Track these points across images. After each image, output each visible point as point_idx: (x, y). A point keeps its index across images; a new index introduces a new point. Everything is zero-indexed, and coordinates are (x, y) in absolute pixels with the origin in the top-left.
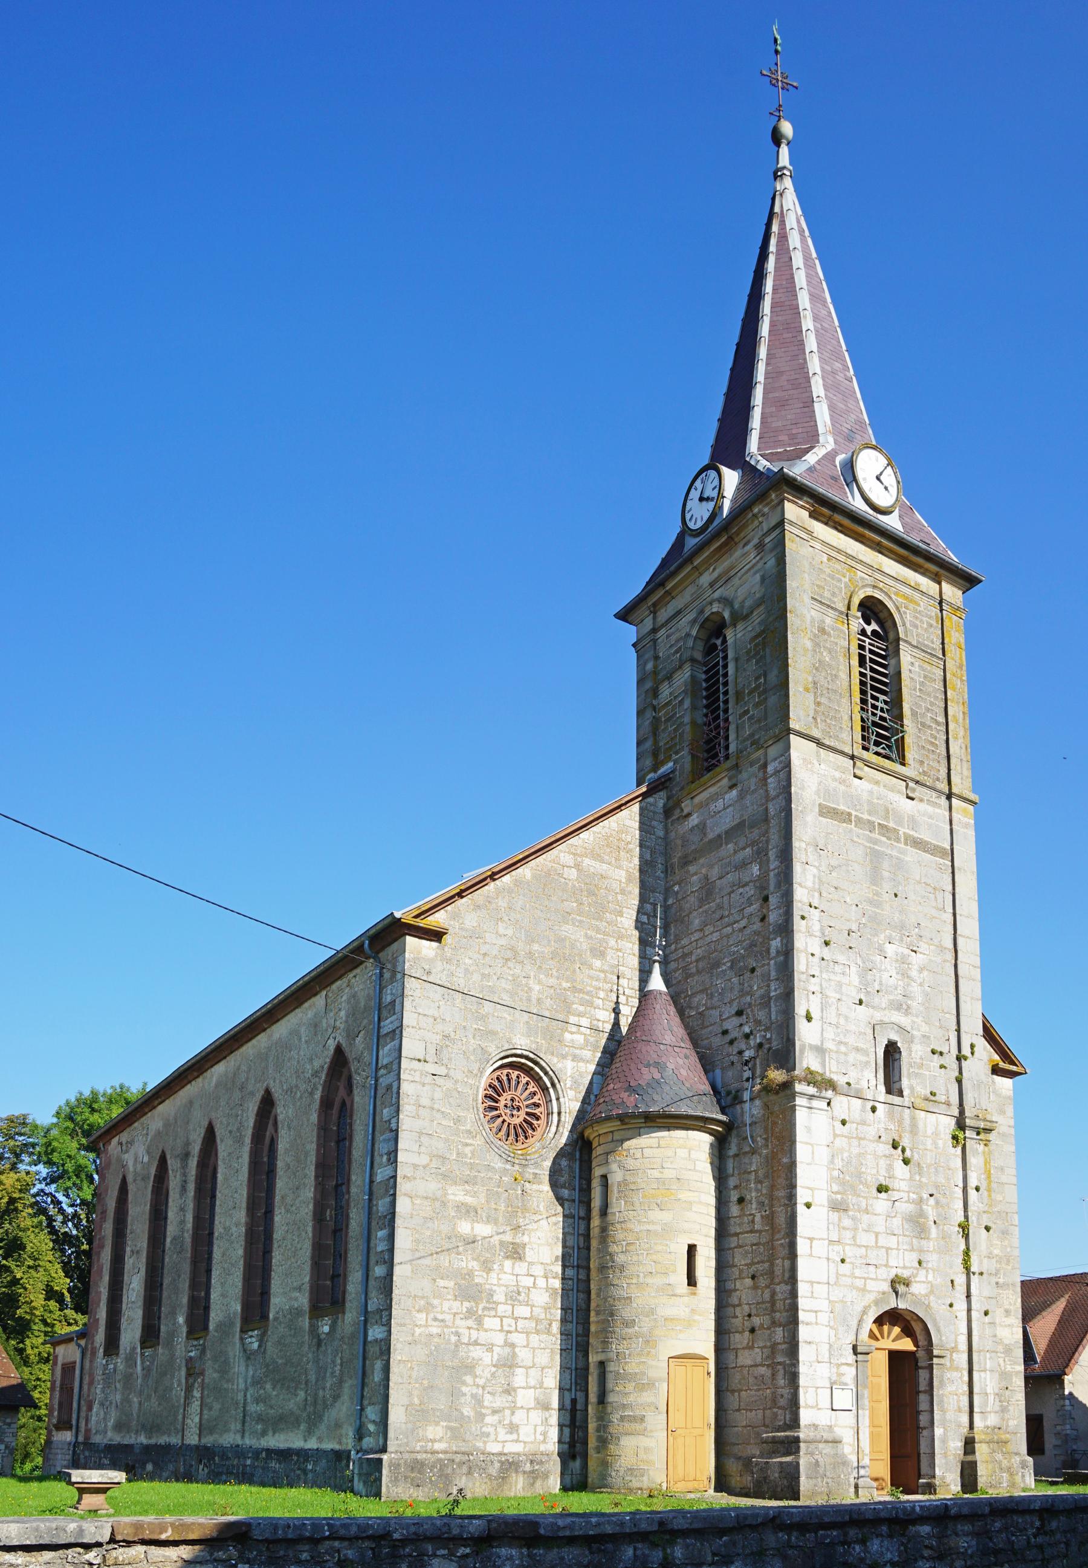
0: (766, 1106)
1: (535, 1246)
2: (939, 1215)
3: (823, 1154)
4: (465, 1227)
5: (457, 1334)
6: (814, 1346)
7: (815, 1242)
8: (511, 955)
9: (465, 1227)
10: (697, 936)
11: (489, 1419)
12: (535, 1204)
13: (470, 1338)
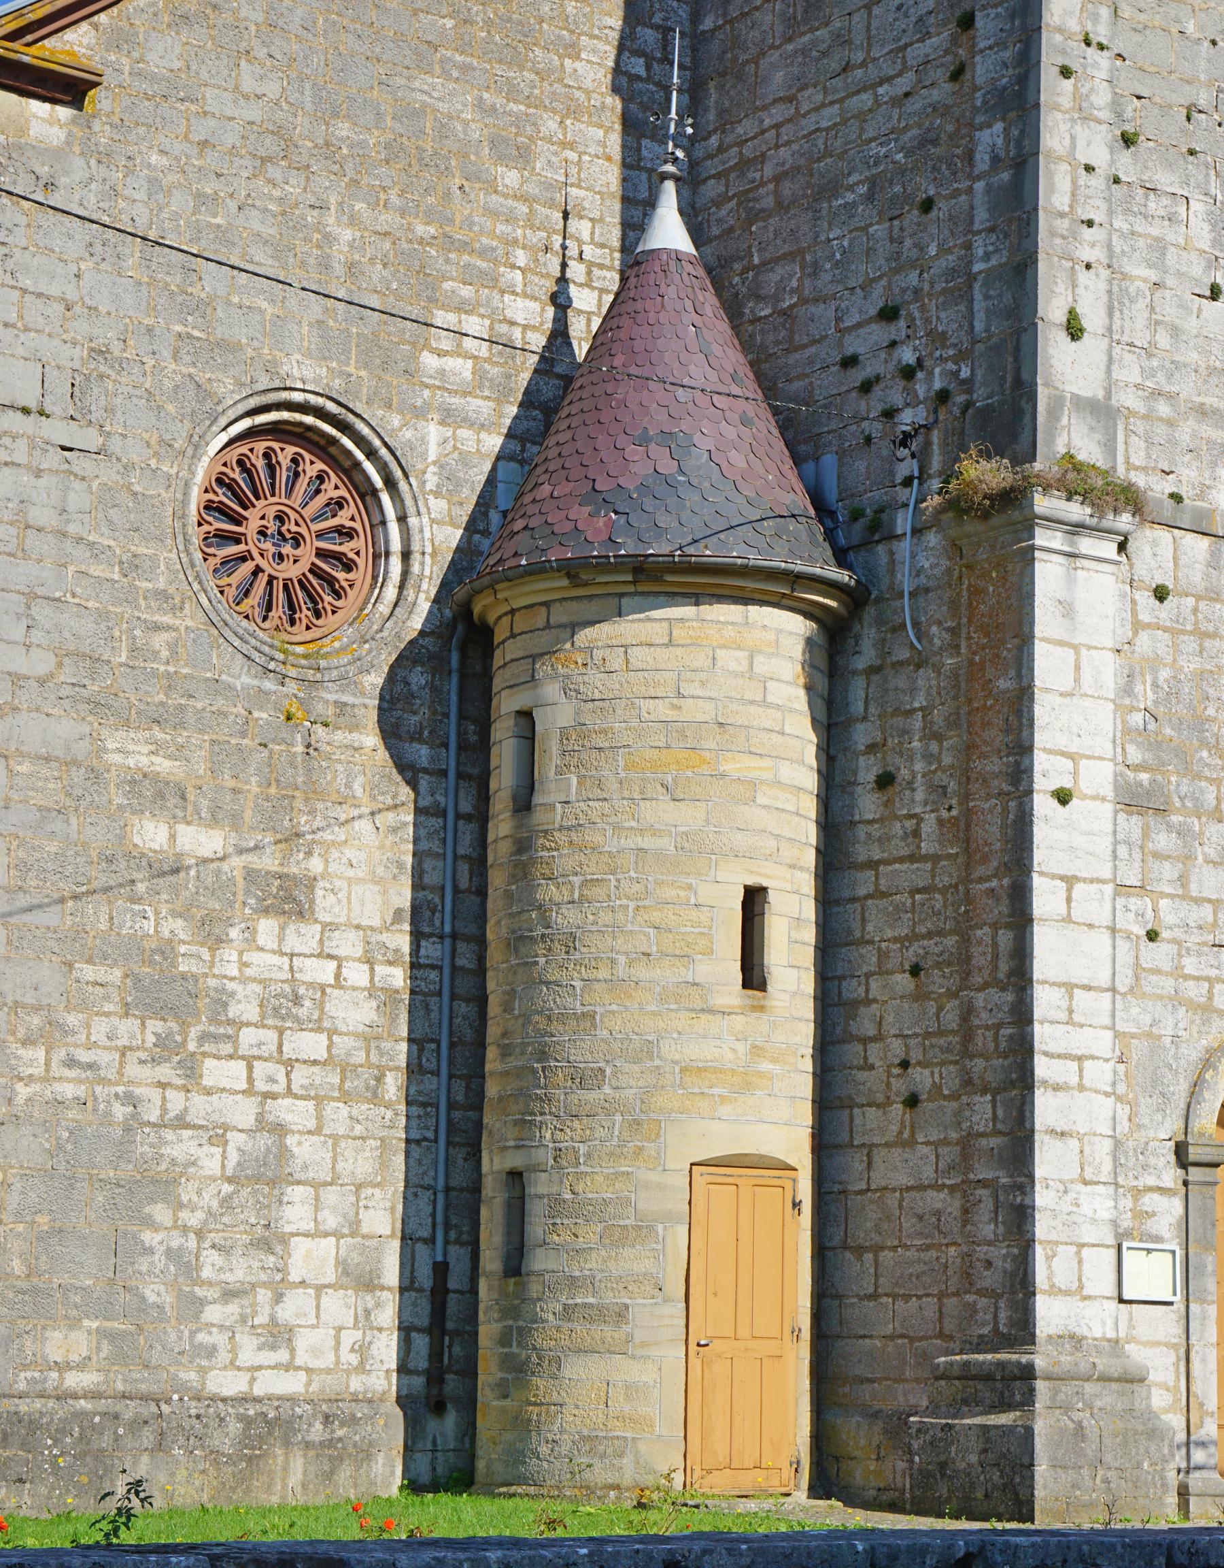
0: (955, 548)
1: (338, 883)
3: (1104, 671)
4: (152, 834)
5: (131, 1100)
6: (1074, 1143)
8: (277, 148)
9: (152, 834)
10: (779, 113)
11: (213, 1313)
12: (341, 779)
13: (164, 1110)
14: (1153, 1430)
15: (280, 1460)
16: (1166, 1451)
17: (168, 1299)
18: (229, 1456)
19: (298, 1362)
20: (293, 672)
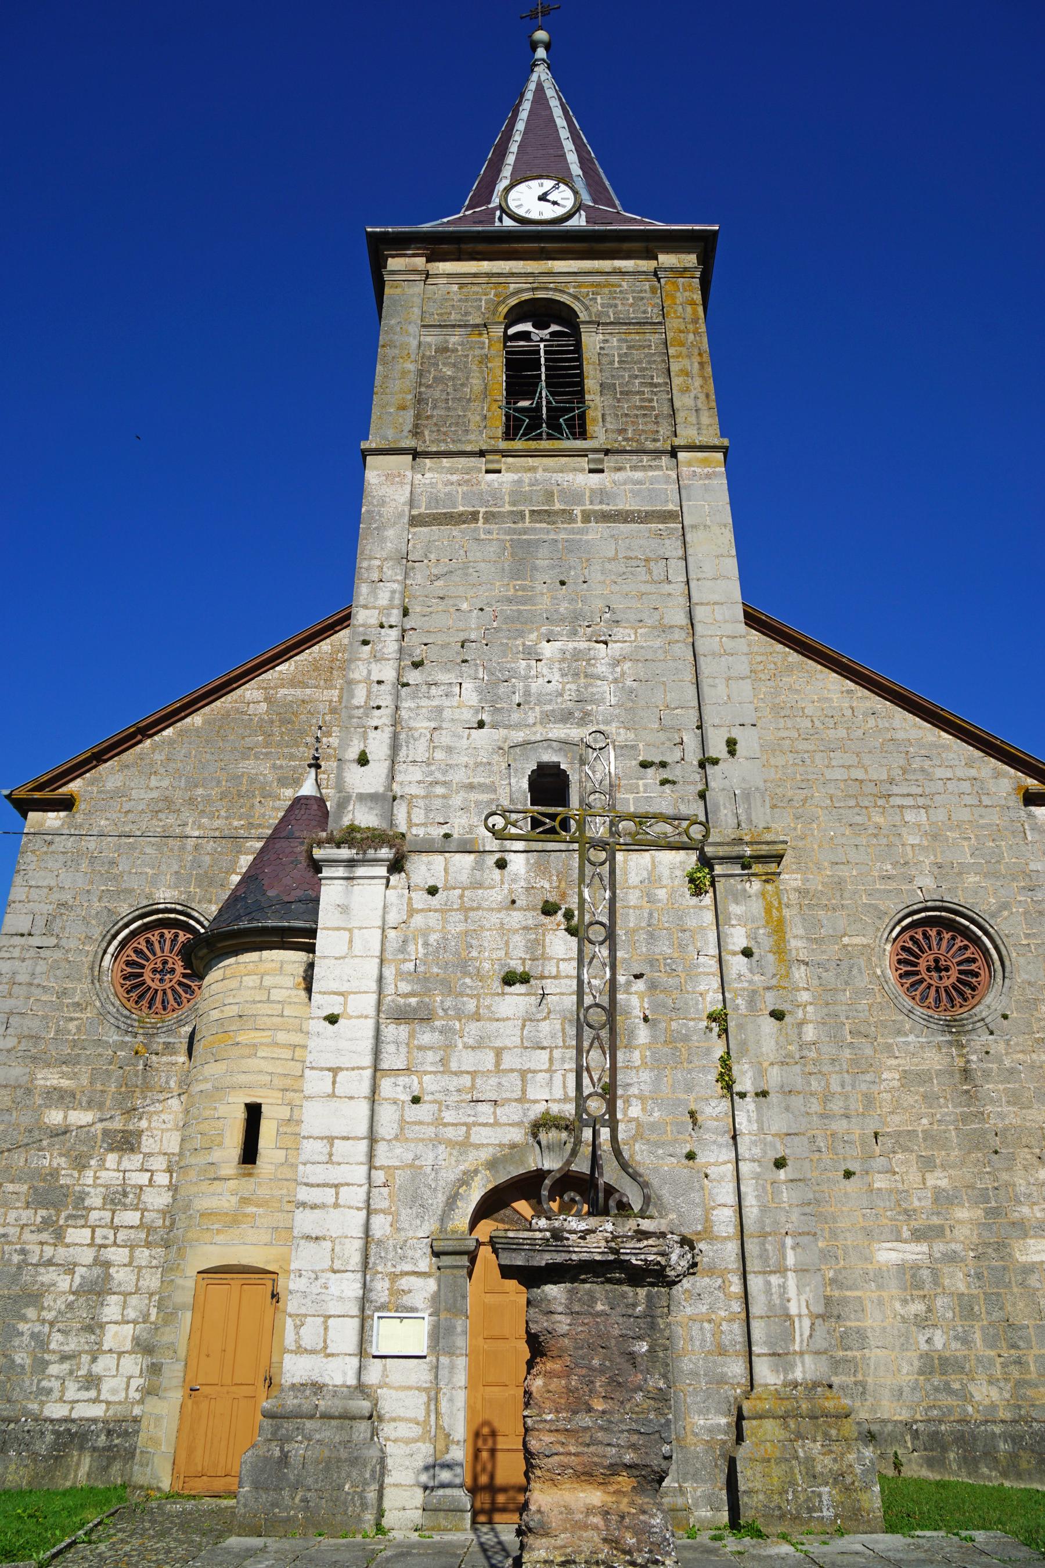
1: (155, 1132)
2: (655, 1006)
5: (23, 1252)
6: (327, 1245)
7: (341, 1076)
9: (55, 1117)
11: (54, 1369)
12: (163, 1080)
13: (41, 1257)
14: (356, 1458)
15: (75, 1459)
16: (368, 1476)
17: (28, 1361)
18: (44, 1456)
19: (102, 1398)
20: (141, 1031)
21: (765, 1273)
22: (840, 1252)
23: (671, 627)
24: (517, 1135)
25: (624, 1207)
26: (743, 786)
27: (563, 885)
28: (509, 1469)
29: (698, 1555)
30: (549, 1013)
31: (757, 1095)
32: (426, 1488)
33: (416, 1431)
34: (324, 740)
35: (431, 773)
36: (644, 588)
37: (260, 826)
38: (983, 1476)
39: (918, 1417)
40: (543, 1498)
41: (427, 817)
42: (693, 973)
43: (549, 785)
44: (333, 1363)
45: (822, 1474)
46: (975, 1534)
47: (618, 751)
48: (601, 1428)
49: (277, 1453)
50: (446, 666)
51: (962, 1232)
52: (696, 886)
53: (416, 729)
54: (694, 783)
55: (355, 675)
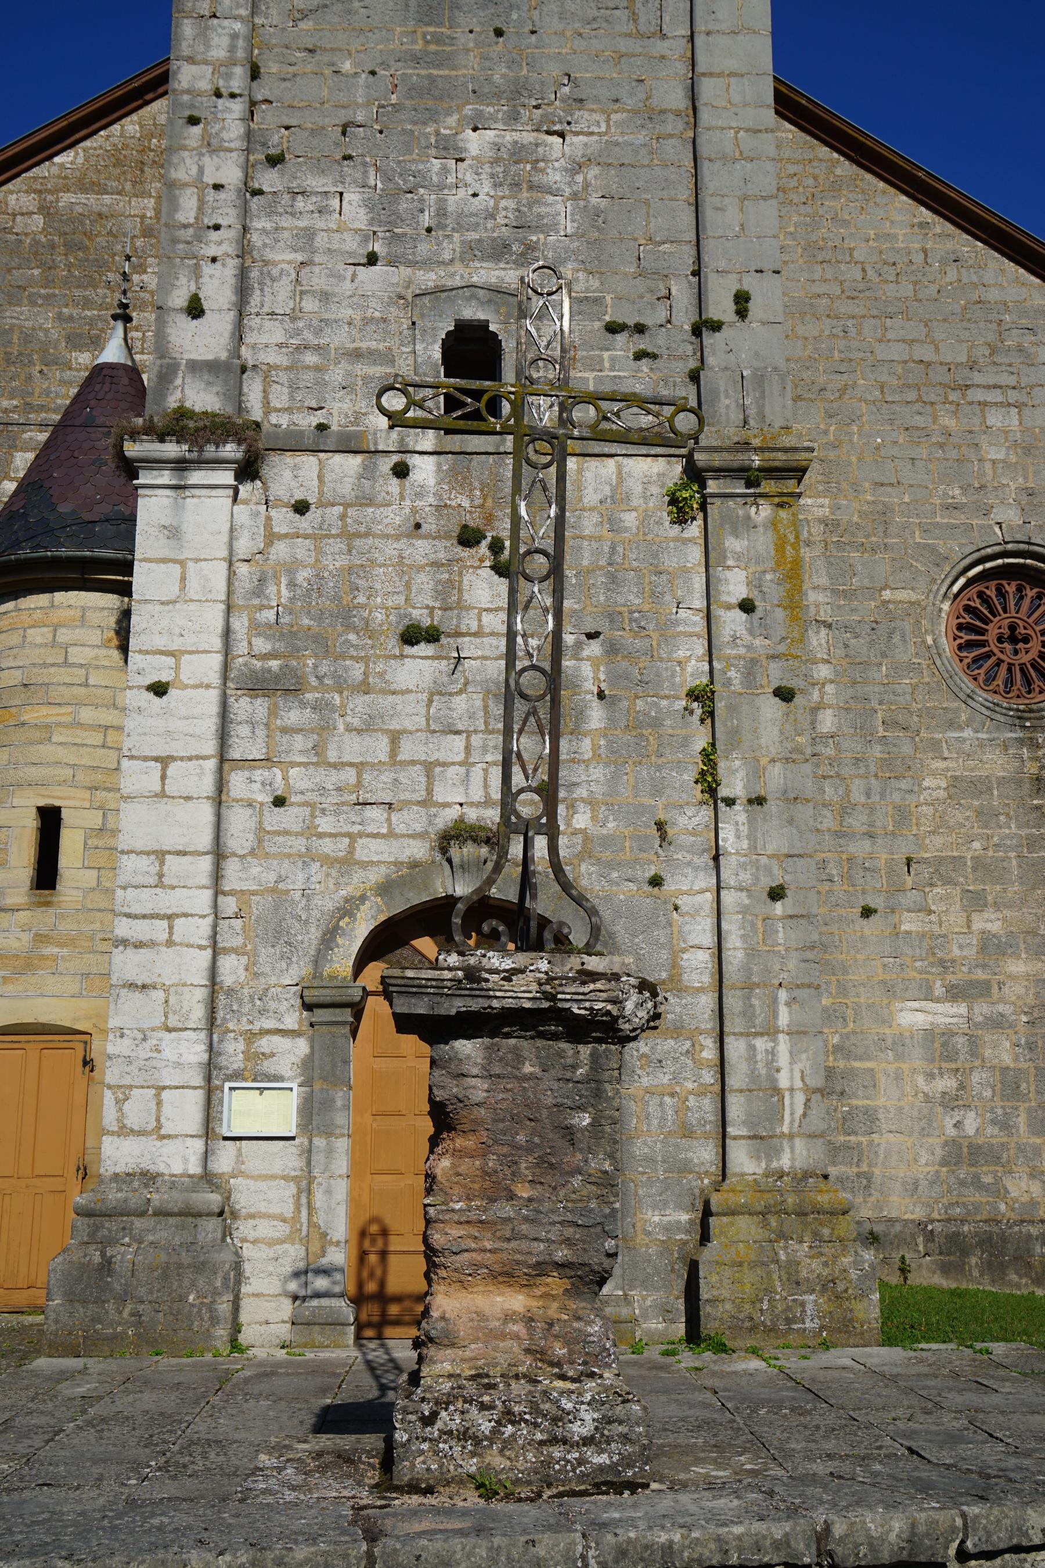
2: (614, 678)
6: (159, 995)
7: (173, 769)
14: (203, 1263)
16: (218, 1284)
21: (748, 1035)
22: (850, 1012)
23: (663, 112)
24: (420, 850)
25: (562, 943)
26: (756, 364)
27: (489, 503)
28: (404, 1274)
29: (644, 1372)
30: (466, 684)
31: (750, 801)
32: (295, 1298)
33: (282, 1230)
34: (136, 278)
35: (298, 332)
36: (623, 45)
37: (42, 408)
38: (1011, 1284)
39: (935, 1215)
40: (447, 1303)
41: (292, 398)
42: (670, 632)
43: (471, 351)
44: (169, 1148)
45: (808, 1280)
46: (991, 1346)
47: (575, 307)
48: (526, 1219)
49: (97, 1258)
50: (319, 164)
51: (1014, 990)
52: (680, 510)
53: (275, 264)
54: (684, 358)
55: (180, 174)
